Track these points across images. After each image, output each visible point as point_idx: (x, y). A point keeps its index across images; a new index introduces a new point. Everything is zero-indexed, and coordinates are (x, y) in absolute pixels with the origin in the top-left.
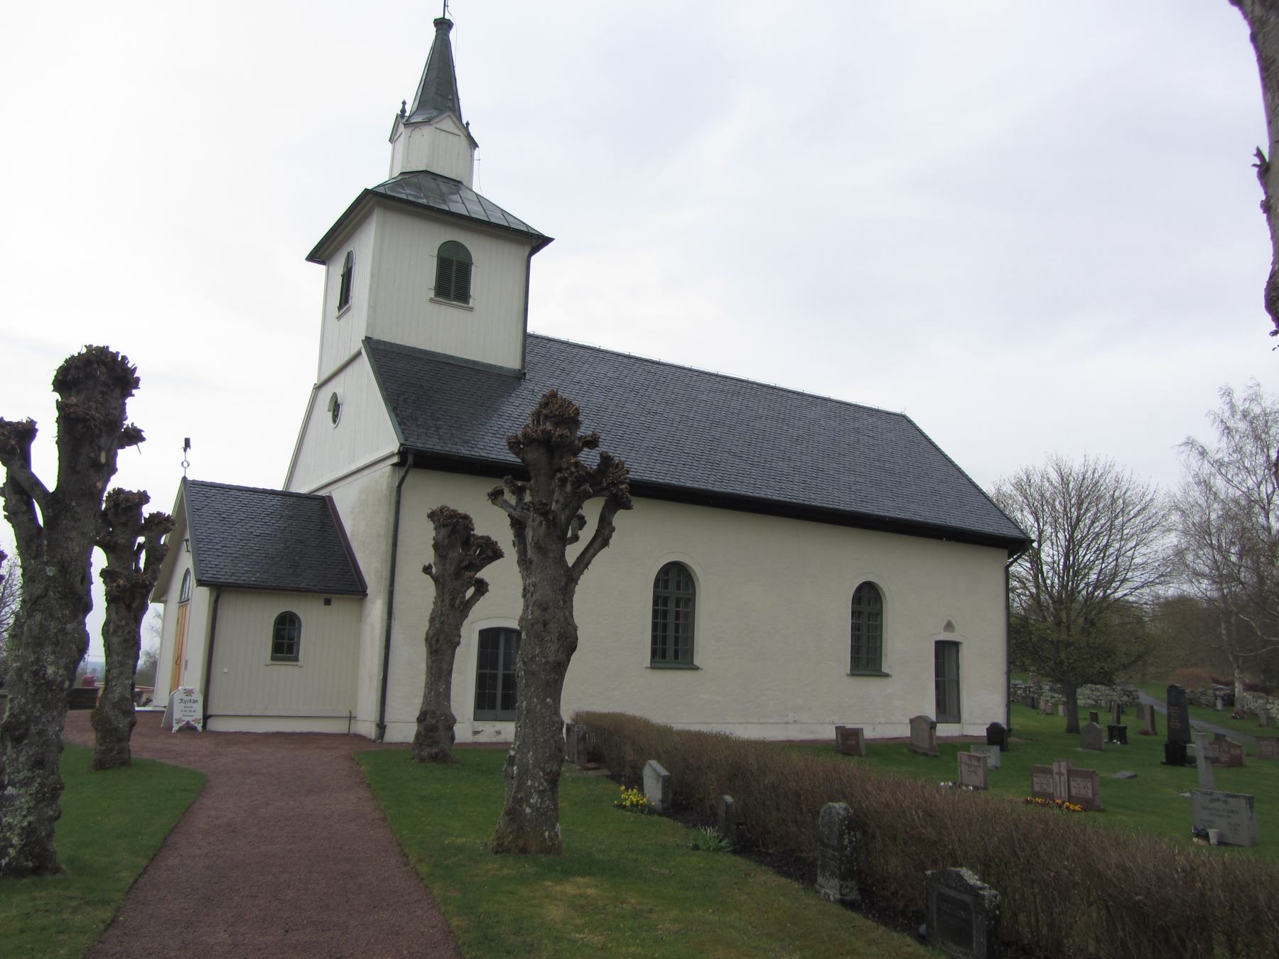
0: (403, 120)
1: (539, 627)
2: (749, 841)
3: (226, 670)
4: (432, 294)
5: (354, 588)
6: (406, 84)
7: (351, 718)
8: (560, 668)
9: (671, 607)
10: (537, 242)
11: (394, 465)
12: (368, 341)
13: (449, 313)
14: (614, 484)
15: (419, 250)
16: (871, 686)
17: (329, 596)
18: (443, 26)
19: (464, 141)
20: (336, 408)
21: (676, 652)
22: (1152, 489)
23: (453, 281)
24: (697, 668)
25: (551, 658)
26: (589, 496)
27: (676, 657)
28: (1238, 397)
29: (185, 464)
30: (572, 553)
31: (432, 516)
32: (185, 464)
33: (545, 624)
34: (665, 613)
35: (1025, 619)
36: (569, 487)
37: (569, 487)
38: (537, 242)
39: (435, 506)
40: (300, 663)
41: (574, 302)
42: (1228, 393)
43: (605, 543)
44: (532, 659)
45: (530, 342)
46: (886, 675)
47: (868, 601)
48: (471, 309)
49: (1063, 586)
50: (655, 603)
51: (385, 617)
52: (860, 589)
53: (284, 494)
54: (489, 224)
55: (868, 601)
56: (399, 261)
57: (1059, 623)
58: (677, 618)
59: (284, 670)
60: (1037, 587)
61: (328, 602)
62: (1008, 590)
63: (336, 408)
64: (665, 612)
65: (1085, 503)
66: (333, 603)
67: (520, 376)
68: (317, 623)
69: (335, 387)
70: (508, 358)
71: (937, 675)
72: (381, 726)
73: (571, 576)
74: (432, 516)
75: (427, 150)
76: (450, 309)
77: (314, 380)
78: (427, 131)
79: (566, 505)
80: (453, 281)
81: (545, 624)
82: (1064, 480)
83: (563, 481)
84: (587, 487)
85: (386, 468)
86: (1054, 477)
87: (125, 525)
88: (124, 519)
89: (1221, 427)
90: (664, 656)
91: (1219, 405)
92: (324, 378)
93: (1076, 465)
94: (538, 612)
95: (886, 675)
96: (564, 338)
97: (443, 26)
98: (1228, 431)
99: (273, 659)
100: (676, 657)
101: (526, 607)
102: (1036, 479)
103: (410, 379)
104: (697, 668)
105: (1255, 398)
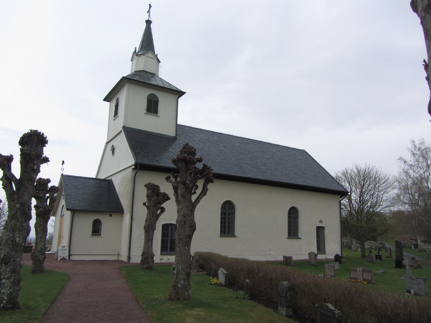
0: (135, 54)
1: (183, 223)
2: (255, 295)
3: (76, 239)
4: (145, 111)
5: (119, 210)
6: (136, 42)
7: (119, 255)
8: (190, 237)
9: (227, 216)
10: (181, 93)
11: (133, 169)
12: (124, 127)
13: (151, 118)
14: (208, 174)
15: (141, 97)
16: (295, 242)
17: (111, 213)
18: (149, 22)
19: (156, 60)
20: (113, 150)
21: (229, 231)
22: (388, 174)
23: (152, 107)
24: (236, 237)
25: (187, 234)
26: (199, 178)
27: (229, 233)
28: (417, 143)
29: (63, 169)
30: (194, 198)
31: (146, 186)
32: (63, 169)
33: (185, 222)
34: (225, 218)
35: (346, 219)
36: (192, 175)
37: (192, 175)
38: (181, 93)
39: (147, 183)
40: (101, 236)
41: (193, 114)
42: (413, 142)
43: (205, 194)
44: (181, 234)
45: (179, 127)
46: (300, 238)
47: (293, 213)
48: (159, 116)
49: (359, 207)
50: (221, 214)
51: (130, 220)
52: (290, 209)
53: (96, 179)
54: (164, 88)
55: (293, 213)
56: (134, 100)
57: (358, 220)
58: (229, 219)
59: (96, 239)
60: (350, 208)
61: (111, 215)
62: (341, 209)
63: (113, 150)
64: (225, 218)
65: (366, 179)
66: (112, 215)
67: (175, 139)
68: (108, 223)
69: (113, 143)
70: (171, 133)
71: (317, 238)
72: (129, 258)
73: (194, 205)
74: (146, 186)
75: (143, 64)
76: (151, 116)
77: (106, 140)
78: (143, 57)
79: (192, 182)
80: (152, 107)
81: (185, 222)
82: (359, 172)
83: (191, 173)
84: (199, 175)
85: (130, 170)
86: (355, 171)
87: (42, 190)
88: (42, 188)
89: (411, 153)
90: (225, 233)
91: (411, 146)
92: (109, 140)
93: (362, 167)
94: (182, 218)
95: (300, 238)
96: (190, 125)
97: (149, 22)
98: (414, 154)
99: (92, 235)
100: (229, 233)
101: (178, 216)
102: (349, 171)
103: (138, 140)
104: (236, 237)
105: (423, 143)
